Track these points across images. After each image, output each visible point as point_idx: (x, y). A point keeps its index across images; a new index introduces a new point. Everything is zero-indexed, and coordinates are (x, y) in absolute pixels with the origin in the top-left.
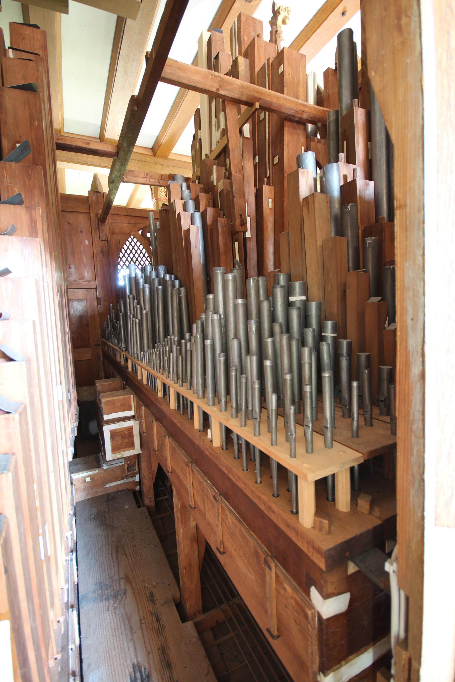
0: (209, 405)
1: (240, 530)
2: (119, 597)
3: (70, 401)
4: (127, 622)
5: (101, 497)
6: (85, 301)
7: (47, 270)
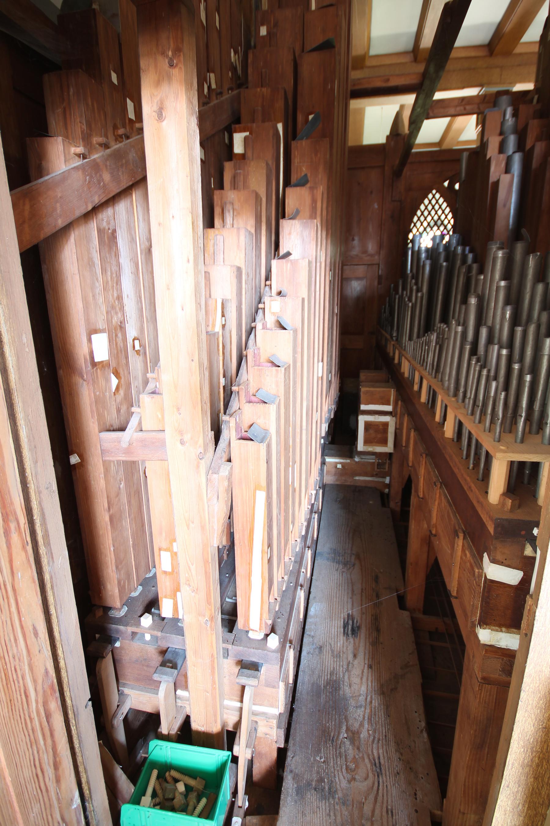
0: (449, 396)
1: (448, 512)
2: (348, 566)
3: (330, 382)
4: (350, 585)
5: (349, 486)
6: (365, 280)
7: (321, 249)
